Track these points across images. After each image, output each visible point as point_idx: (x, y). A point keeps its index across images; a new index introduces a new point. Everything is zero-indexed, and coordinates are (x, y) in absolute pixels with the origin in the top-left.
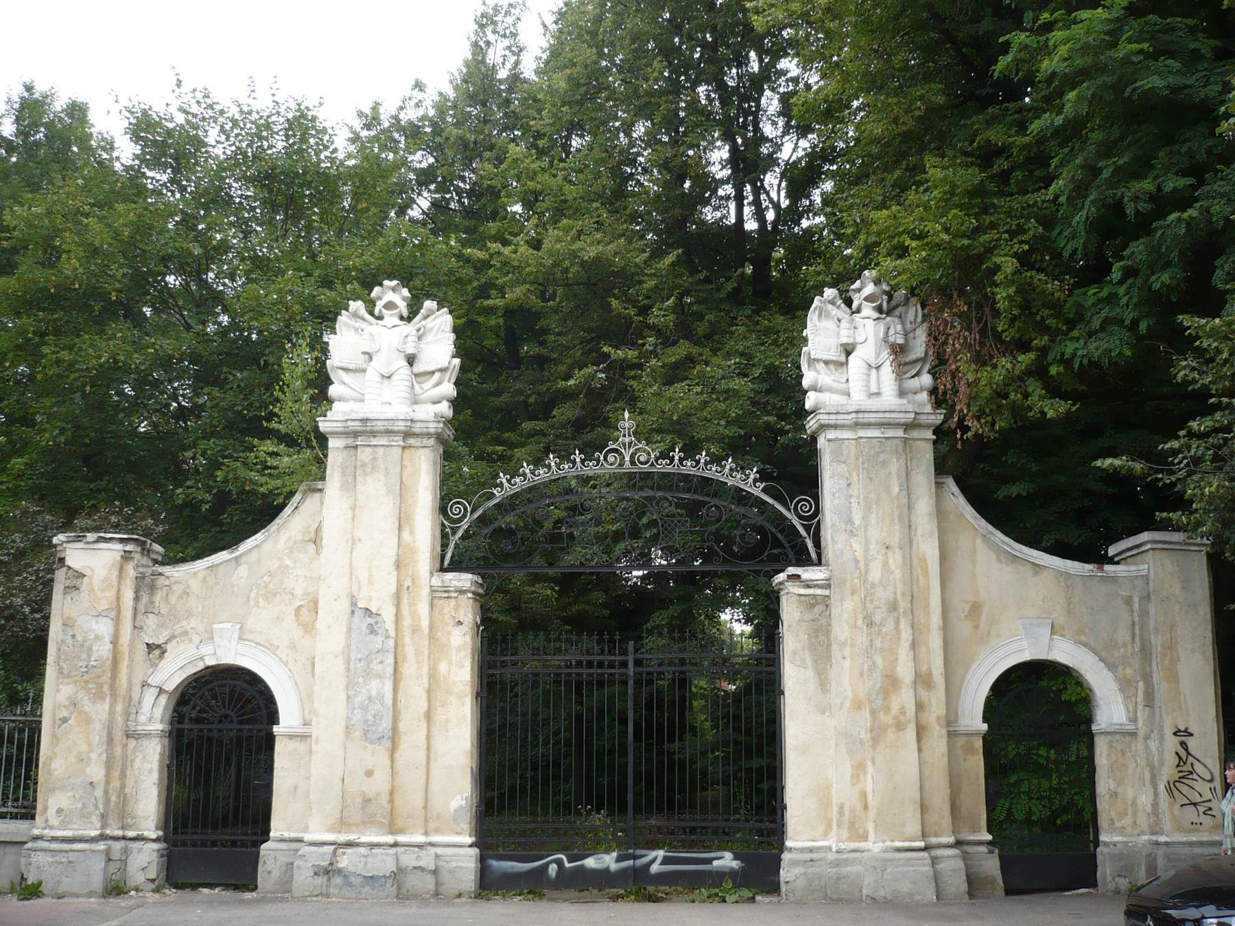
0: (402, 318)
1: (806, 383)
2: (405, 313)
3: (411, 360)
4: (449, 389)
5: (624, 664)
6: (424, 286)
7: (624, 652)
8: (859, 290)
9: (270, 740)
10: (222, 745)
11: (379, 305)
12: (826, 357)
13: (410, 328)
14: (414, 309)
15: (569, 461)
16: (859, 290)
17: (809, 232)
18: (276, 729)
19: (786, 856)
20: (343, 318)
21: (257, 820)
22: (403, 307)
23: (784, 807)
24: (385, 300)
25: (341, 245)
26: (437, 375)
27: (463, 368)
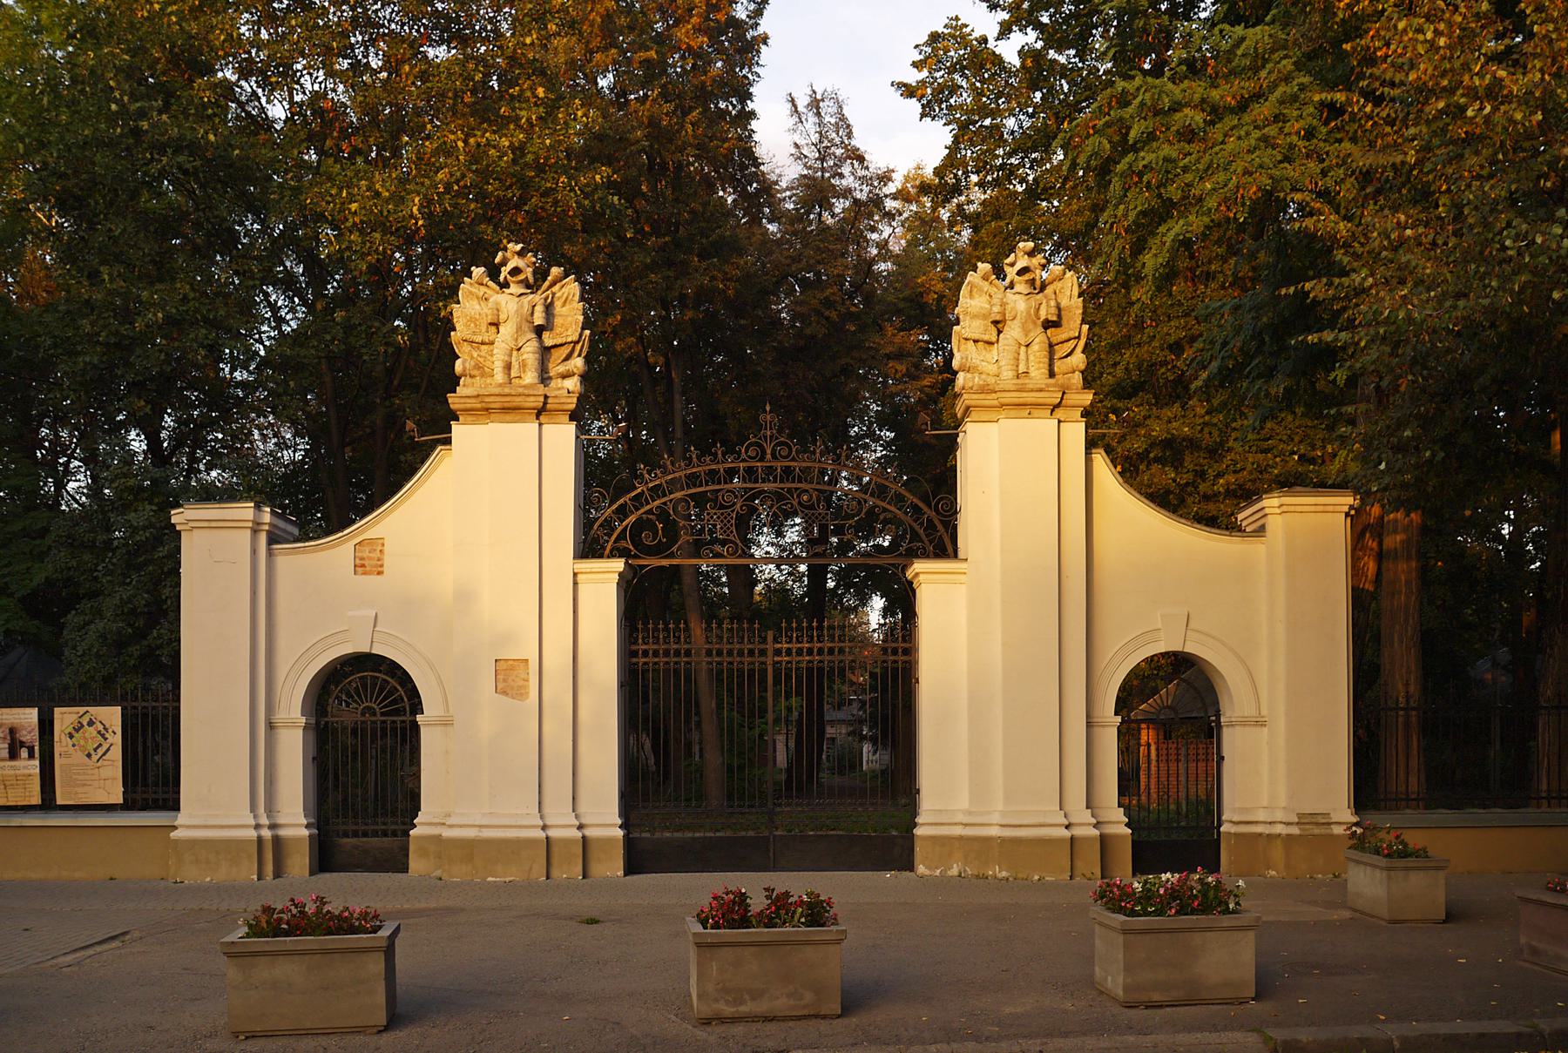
0: (528, 286)
1: (955, 364)
2: (531, 280)
3: (539, 331)
4: (578, 363)
5: (763, 653)
6: (553, 250)
7: (764, 640)
8: (1012, 265)
9: (415, 728)
10: (366, 725)
11: (505, 271)
12: (976, 336)
13: (538, 298)
14: (541, 274)
15: (711, 454)
16: (1012, 265)
17: (517, 242)
18: (419, 718)
19: (918, 831)
20: (466, 287)
21: (405, 801)
22: (528, 273)
23: (918, 791)
24: (510, 266)
25: (1356, 350)
26: (565, 351)
27: (593, 342)
